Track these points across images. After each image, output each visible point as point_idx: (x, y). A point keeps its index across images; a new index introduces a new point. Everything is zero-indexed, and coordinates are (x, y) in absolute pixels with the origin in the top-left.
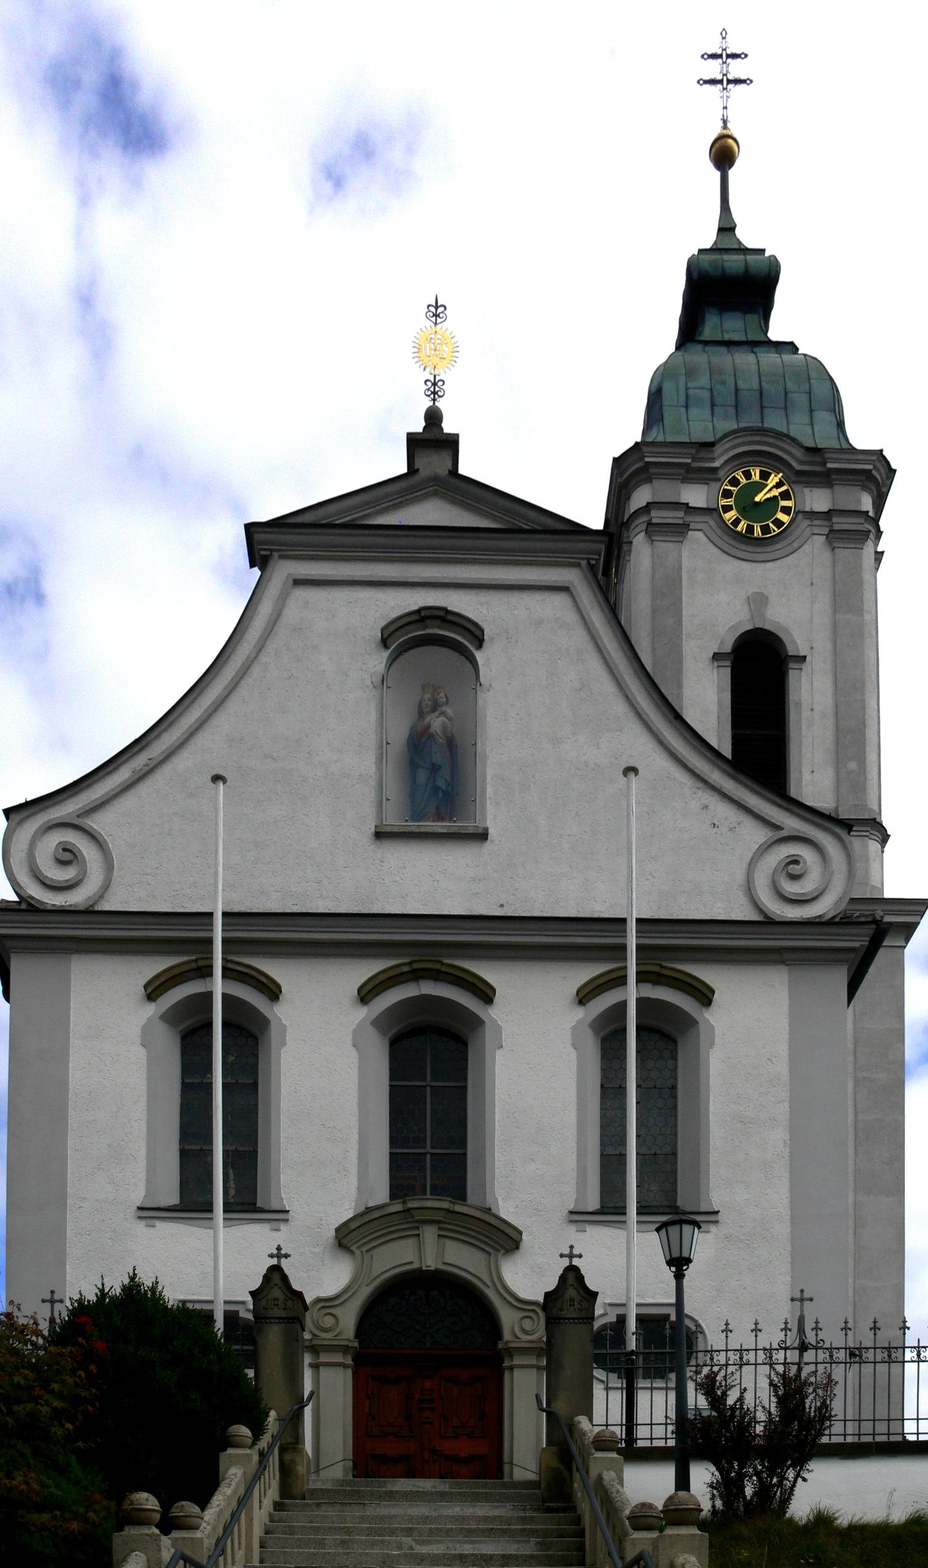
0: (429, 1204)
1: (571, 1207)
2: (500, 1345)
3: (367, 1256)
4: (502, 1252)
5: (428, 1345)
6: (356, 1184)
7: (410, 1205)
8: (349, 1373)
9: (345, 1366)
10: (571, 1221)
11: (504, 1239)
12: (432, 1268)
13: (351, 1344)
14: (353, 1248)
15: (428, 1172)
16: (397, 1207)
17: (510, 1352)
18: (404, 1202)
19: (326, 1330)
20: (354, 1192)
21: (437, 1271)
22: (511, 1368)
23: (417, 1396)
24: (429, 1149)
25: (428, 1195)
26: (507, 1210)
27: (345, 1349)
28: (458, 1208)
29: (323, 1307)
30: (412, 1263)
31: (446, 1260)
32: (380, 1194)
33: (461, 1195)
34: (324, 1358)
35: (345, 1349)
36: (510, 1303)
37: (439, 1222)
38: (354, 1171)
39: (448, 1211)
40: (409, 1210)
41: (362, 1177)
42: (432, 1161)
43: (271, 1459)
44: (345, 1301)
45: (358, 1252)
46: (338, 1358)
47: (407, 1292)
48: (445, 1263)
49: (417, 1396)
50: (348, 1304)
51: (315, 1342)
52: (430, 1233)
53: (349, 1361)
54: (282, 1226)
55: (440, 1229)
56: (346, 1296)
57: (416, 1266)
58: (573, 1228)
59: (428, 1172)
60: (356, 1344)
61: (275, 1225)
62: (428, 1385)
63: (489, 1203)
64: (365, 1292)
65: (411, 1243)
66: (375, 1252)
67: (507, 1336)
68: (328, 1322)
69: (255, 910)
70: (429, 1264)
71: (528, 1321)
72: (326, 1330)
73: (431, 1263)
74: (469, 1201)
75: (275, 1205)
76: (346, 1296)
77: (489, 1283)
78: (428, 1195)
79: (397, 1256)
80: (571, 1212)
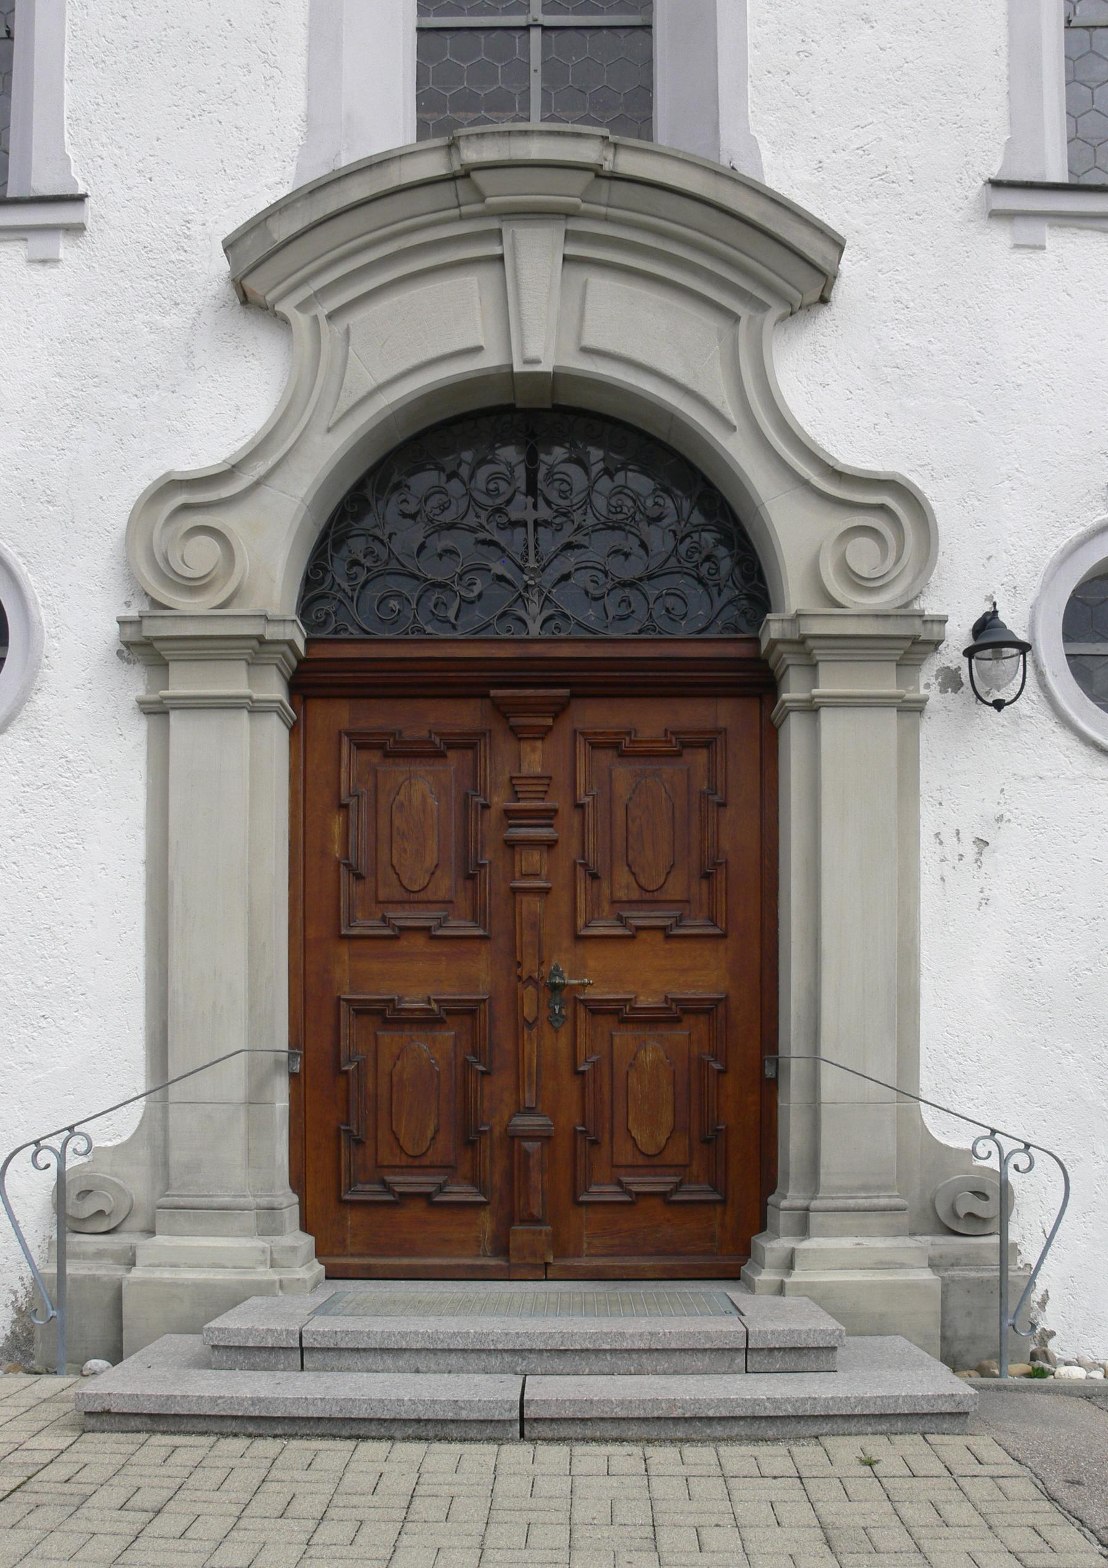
0: (536, 149)
1: (995, 173)
2: (774, 628)
3: (331, 333)
4: (777, 310)
5: (534, 629)
6: (302, 105)
7: (472, 154)
8: (275, 735)
9: (255, 708)
10: (996, 215)
11: (779, 264)
12: (546, 367)
13: (271, 632)
14: (286, 307)
15: (536, 84)
16: (433, 165)
17: (807, 650)
18: (452, 146)
19: (194, 586)
20: (293, 133)
21: (559, 379)
22: (812, 708)
23: (500, 800)
24: (536, 14)
25: (536, 123)
26: (786, 172)
27: (256, 650)
28: (629, 164)
29: (186, 508)
30: (478, 350)
31: (591, 340)
32: (382, 114)
33: (633, 114)
34: (185, 682)
35: (256, 650)
36: (806, 484)
37: (568, 214)
38: (295, 62)
39: (598, 173)
40: (465, 174)
41: (322, 76)
42: (545, 47)
43: (470, 1189)
44: (257, 484)
45: (301, 321)
46: (232, 681)
47: (467, 456)
48: (587, 351)
49: (500, 800)
50: (268, 495)
51: (152, 629)
52: (536, 252)
53: (275, 689)
54: (64, 248)
55: (570, 236)
56: (260, 468)
57: (490, 360)
58: (1001, 236)
59: (536, 84)
60: (298, 636)
61: (39, 245)
62: (534, 759)
63: (730, 151)
64: (323, 455)
65: (472, 287)
66: (356, 319)
67: (794, 594)
68: (201, 555)
69: (698, 1282)
70: (533, 352)
71: (865, 543)
72: (194, 586)
73: (543, 349)
74: (663, 134)
75: (43, 184)
76: (260, 468)
77: (731, 412)
78: (536, 123)
79: (438, 331)
80: (996, 184)
